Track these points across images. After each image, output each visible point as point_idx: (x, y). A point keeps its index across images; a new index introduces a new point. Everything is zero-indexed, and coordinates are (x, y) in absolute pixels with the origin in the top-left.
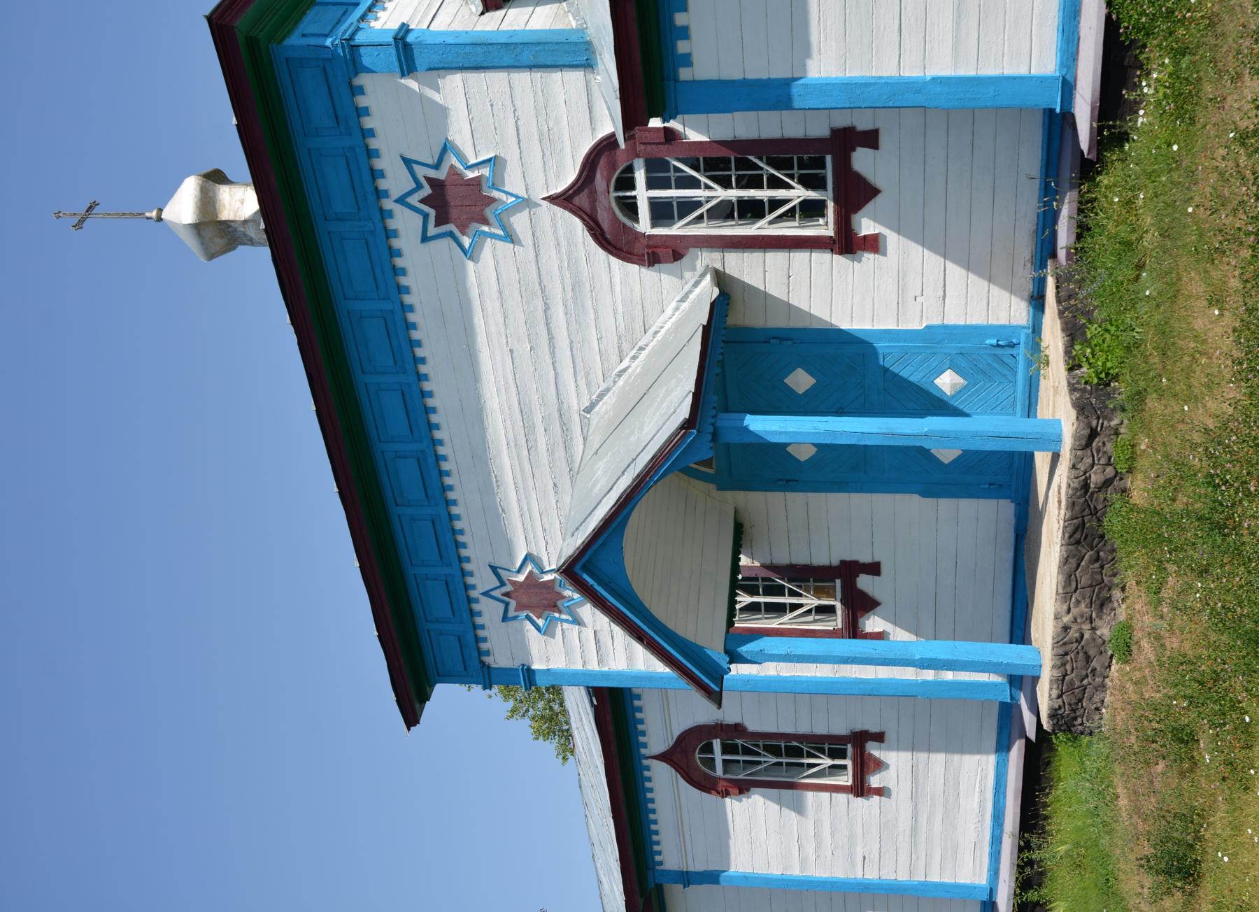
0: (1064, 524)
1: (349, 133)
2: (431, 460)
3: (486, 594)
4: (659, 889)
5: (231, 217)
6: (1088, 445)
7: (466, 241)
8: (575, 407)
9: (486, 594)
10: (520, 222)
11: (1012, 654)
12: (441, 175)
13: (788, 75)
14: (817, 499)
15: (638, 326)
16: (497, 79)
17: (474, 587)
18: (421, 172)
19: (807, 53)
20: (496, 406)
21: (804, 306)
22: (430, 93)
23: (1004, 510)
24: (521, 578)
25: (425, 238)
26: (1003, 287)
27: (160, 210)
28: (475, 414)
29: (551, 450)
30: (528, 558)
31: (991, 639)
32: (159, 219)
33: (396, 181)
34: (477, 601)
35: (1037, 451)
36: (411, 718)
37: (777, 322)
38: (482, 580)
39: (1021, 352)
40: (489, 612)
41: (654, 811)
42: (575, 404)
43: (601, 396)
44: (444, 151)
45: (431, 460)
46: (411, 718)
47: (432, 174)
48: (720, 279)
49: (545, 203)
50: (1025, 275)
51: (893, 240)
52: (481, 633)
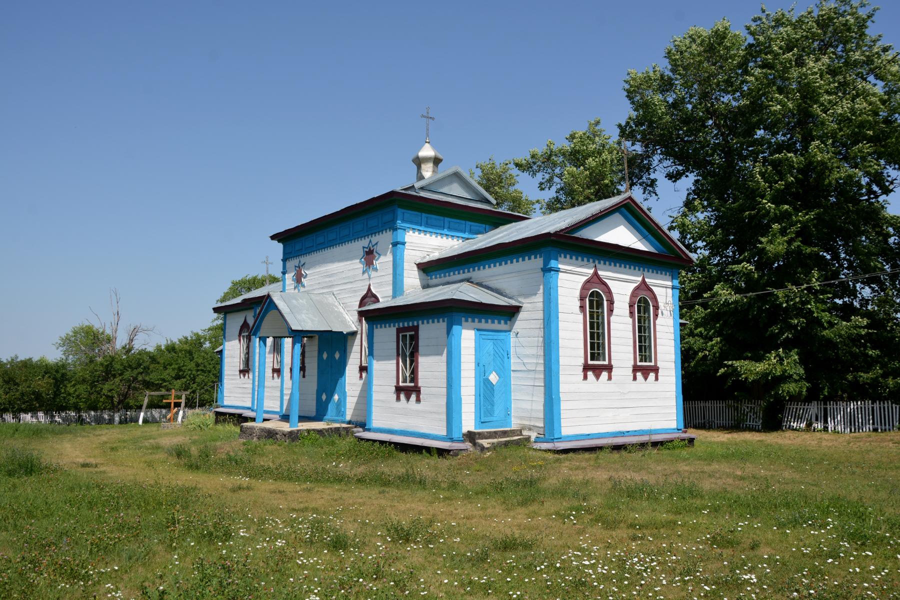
0: (303, 430)
1: (382, 227)
2: (324, 246)
3: (370, 241)
4: (252, 308)
5: (422, 168)
6: (283, 434)
7: (363, 260)
8: (335, 290)
9: (370, 241)
10: (366, 275)
11: (294, 417)
12: (375, 253)
13: (374, 355)
14: (316, 359)
15: (349, 309)
16: (391, 271)
17: (372, 237)
18: (375, 247)
19: (377, 361)
20: (322, 269)
21: (351, 357)
22: (389, 250)
23: (313, 414)
24: (303, 272)
25: (364, 247)
26: (353, 413)
27: (429, 143)
28: (332, 261)
29: (326, 282)
30: (307, 274)
31: (299, 411)
32: (426, 142)
33: (374, 239)
34: (368, 238)
35: (461, 428)
36: (273, 237)
37: (348, 348)
38: (303, 259)
39: (341, 418)
40: (365, 242)
41: (529, 259)
42: (335, 289)
43: (336, 297)
44: (379, 254)
45: (324, 246)
46: (273, 237)
47: (375, 251)
48: (354, 334)
49: (368, 283)
50: (354, 419)
51: (362, 382)
52: (377, 234)
